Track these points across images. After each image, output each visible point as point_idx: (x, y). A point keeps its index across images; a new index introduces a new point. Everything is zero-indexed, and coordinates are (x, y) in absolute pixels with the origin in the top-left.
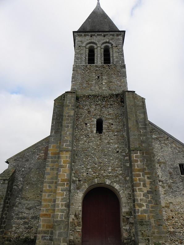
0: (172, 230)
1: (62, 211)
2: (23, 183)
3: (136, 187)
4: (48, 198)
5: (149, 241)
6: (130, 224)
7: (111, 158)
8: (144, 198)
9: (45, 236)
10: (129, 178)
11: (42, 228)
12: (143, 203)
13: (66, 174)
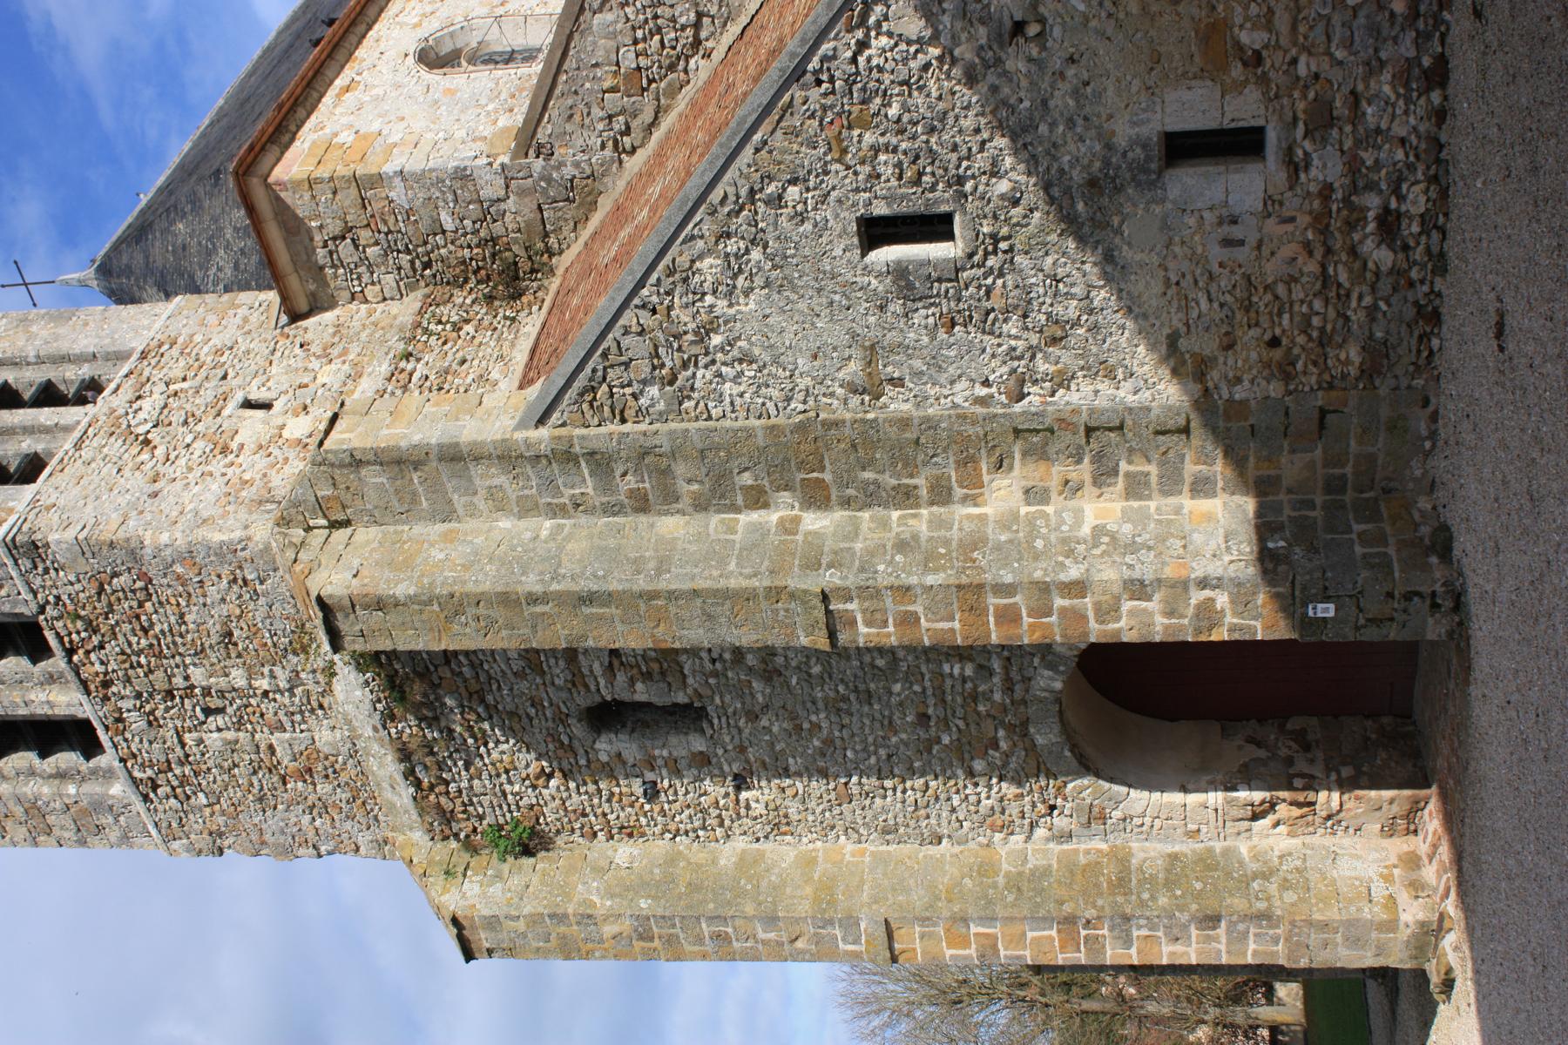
3: (1086, 634)
5: (1417, 594)
8: (1157, 597)
12: (1193, 602)
13: (1030, 935)
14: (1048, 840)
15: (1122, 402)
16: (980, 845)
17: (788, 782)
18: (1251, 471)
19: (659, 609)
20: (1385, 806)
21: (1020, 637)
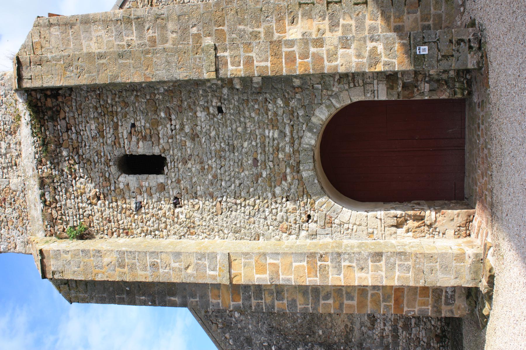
1: (391, 268)
2: (310, 344)
3: (323, 68)
4: (356, 299)
5: (462, 40)
6: (417, 81)
8: (353, 46)
9: (446, 297)
12: (368, 49)
13: (295, 264)
14: (306, 237)
16: (277, 240)
17: (197, 201)
18: (393, 24)
19: (148, 59)
20: (456, 218)
21: (295, 70)
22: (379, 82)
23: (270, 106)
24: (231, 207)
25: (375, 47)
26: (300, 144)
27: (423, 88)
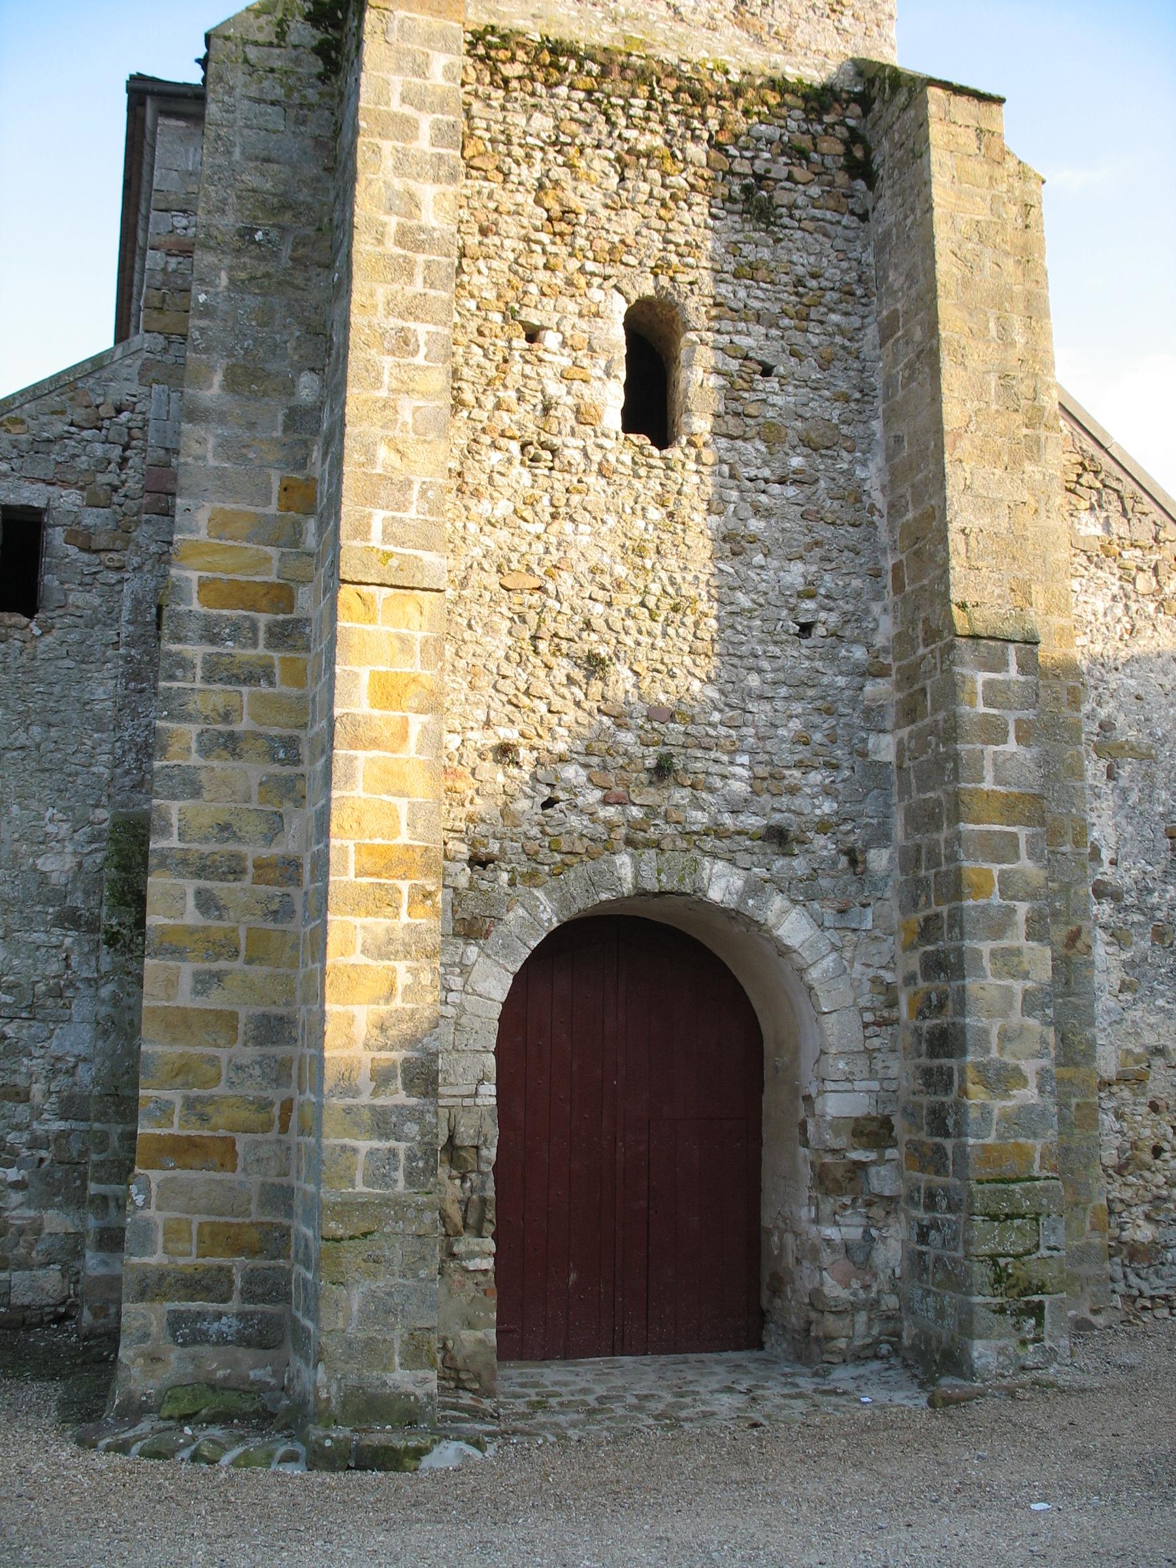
0: (1144, 1233)
4: (200, 1003)
6: (869, 1204)
7: (754, 680)
9: (200, 1315)
10: (891, 858)
11: (166, 1251)
13: (402, 805)
15: (1096, 998)
22: (874, 1095)
23: (815, 777)
24: (524, 622)
25: (1023, 1081)
26: (715, 856)
27: (848, 1221)
